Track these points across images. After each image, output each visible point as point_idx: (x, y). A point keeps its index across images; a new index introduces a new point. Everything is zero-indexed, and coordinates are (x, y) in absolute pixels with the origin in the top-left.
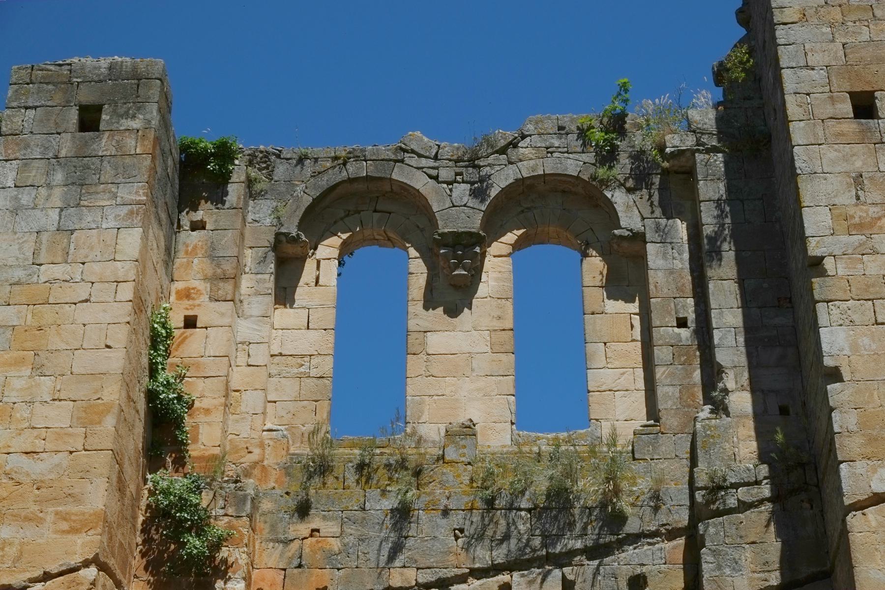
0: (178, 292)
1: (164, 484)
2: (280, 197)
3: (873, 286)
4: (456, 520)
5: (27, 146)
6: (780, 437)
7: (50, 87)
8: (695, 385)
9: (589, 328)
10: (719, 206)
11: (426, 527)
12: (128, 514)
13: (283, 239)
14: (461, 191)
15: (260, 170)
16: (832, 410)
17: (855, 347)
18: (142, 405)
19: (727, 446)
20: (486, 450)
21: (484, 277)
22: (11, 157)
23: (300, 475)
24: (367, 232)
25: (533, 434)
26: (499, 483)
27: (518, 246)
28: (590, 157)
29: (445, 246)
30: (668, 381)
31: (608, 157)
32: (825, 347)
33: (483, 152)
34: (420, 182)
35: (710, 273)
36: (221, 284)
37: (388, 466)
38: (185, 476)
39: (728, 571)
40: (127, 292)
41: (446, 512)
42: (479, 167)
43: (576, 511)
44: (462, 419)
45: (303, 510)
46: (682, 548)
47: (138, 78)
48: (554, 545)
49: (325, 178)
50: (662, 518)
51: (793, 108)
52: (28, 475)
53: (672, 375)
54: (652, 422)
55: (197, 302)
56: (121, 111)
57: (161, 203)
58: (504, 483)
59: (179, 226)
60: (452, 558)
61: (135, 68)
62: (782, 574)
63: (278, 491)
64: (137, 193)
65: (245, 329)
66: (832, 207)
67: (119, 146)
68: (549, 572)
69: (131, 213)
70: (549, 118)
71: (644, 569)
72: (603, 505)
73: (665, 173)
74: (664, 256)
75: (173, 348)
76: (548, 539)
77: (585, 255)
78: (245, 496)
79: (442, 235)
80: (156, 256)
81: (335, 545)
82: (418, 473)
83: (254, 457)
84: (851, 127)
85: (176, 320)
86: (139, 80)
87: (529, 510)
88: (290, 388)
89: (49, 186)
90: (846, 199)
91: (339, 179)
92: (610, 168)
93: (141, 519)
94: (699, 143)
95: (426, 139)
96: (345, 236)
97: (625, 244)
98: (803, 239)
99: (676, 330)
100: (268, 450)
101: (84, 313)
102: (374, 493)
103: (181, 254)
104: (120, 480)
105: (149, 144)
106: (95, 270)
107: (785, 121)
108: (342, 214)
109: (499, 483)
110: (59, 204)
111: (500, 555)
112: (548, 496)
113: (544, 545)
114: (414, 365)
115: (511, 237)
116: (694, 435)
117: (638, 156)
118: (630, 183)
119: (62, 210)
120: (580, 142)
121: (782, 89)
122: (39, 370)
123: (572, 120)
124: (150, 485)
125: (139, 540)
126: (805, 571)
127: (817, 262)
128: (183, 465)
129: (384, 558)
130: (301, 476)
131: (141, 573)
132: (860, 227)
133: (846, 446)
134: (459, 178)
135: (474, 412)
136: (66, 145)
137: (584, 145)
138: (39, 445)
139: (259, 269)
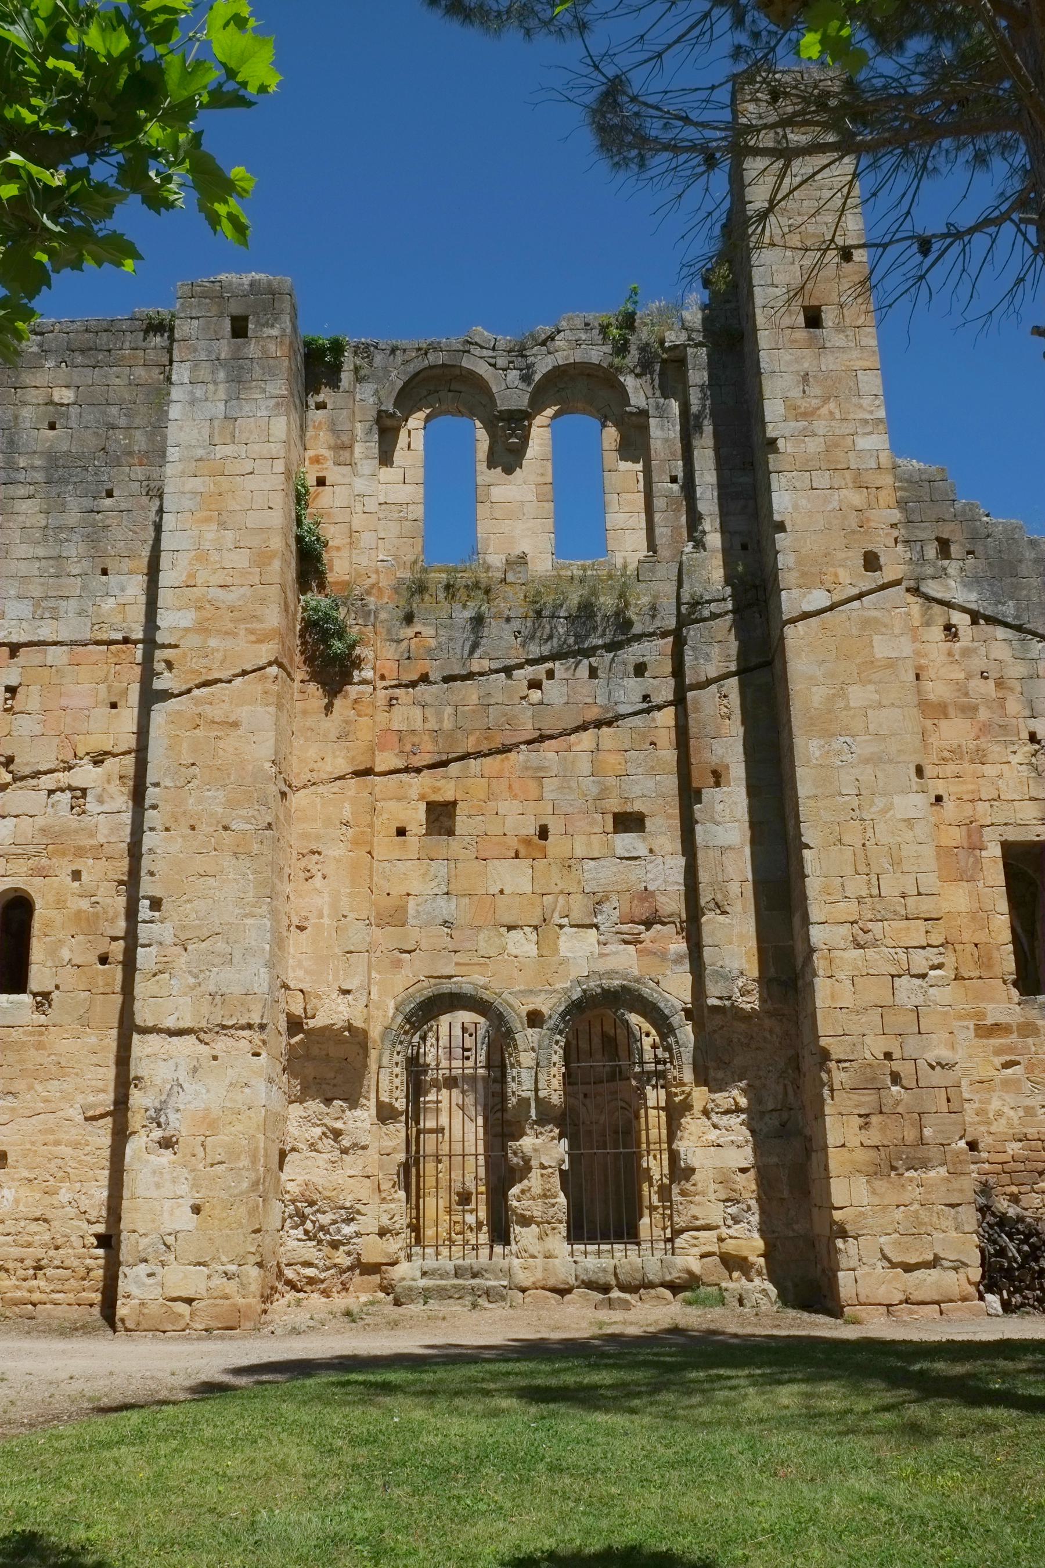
0: (310, 458)
1: (313, 603)
2: (379, 380)
3: (812, 460)
4: (516, 625)
5: (195, 350)
6: (740, 569)
7: (208, 301)
8: (681, 527)
9: (607, 482)
10: (702, 391)
11: (495, 631)
12: (291, 625)
13: (384, 415)
14: (513, 375)
15: (363, 358)
16: (778, 552)
17: (796, 507)
18: (294, 548)
19: (704, 572)
20: (534, 574)
21: (530, 442)
22: (185, 359)
23: (405, 593)
24: (444, 407)
25: (567, 562)
26: (545, 599)
27: (554, 417)
28: (608, 349)
29: (503, 420)
30: (663, 524)
31: (621, 349)
32: (775, 507)
33: (530, 343)
34: (483, 369)
35: (695, 443)
36: (341, 452)
37: (467, 587)
38: (326, 596)
39: (702, 661)
40: (279, 466)
41: (508, 620)
42: (526, 356)
43: (598, 619)
44: (518, 552)
45: (409, 619)
46: (671, 644)
47: (273, 293)
48: (583, 642)
49: (412, 366)
50: (658, 623)
51: (760, 320)
52: (224, 602)
53: (666, 519)
54: (651, 553)
55: (325, 466)
56: (263, 321)
57: (296, 392)
58: (549, 599)
59: (307, 406)
60: (513, 651)
61: (269, 283)
62: (738, 664)
63: (391, 605)
64: (280, 388)
65: (360, 485)
66: (786, 399)
67: (264, 350)
68: (580, 661)
69: (278, 404)
70: (578, 316)
71: (645, 659)
72: (617, 614)
73: (664, 362)
74: (662, 429)
75: (310, 502)
76: (579, 638)
77: (604, 426)
78: (370, 611)
79: (500, 412)
80: (295, 433)
81: (433, 643)
82: (487, 592)
83: (373, 579)
84: (802, 334)
85: (311, 481)
86: (274, 295)
87: (566, 618)
88: (394, 528)
89: (215, 383)
90: (796, 393)
91: (422, 366)
92: (624, 358)
93: (298, 627)
94: (690, 339)
95: (486, 333)
96: (428, 411)
97: (634, 418)
98: (763, 424)
99: (670, 485)
100: (382, 576)
101: (250, 483)
102: (458, 606)
103: (310, 429)
104: (286, 604)
105: (286, 348)
106: (256, 449)
107: (755, 330)
108: (425, 393)
109: (545, 599)
110: (224, 397)
111: (546, 650)
112: (579, 608)
113: (576, 643)
114: (482, 510)
115: (550, 412)
116: (681, 564)
117: (644, 349)
118: (638, 370)
119: (226, 402)
120: (601, 336)
121: (753, 303)
122: (223, 526)
123: (595, 317)
124: (302, 603)
125: (299, 642)
126: (754, 661)
127: (773, 442)
128: (324, 588)
129: (466, 653)
130: (406, 594)
131: (301, 665)
132: (807, 415)
133: (787, 578)
134: (511, 366)
135: (524, 546)
136: (224, 348)
137: (604, 338)
138: (229, 581)
139: (367, 439)
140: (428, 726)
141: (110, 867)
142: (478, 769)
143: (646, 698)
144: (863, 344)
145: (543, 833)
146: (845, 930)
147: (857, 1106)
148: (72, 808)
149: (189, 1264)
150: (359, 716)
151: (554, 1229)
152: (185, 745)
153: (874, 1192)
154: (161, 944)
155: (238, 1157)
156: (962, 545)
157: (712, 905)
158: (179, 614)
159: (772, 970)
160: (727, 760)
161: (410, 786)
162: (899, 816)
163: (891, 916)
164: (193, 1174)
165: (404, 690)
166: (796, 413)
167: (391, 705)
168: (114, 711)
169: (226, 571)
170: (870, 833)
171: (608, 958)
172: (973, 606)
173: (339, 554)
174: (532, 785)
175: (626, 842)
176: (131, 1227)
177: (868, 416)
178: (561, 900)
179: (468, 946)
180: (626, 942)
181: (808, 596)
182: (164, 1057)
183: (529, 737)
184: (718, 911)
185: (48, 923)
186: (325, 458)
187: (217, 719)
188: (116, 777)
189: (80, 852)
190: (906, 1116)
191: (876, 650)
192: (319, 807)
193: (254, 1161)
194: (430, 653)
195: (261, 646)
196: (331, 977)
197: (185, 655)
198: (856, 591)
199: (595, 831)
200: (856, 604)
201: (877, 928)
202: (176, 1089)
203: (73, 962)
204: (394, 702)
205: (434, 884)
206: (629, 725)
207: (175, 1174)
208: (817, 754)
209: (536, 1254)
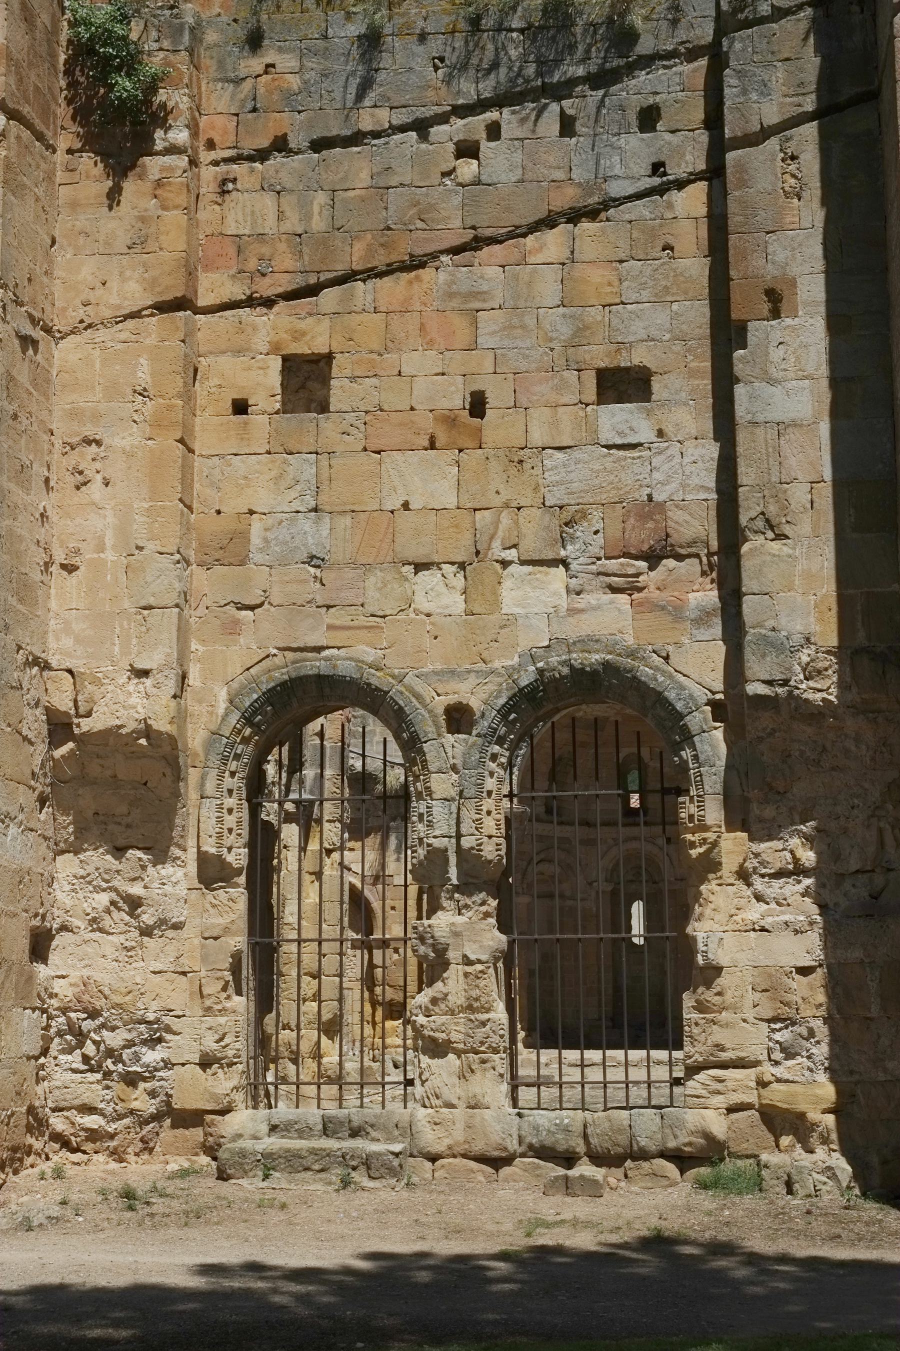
81: (294, 82)
140: (287, 226)
142: (370, 298)
143: (657, 168)
150: (164, 208)
151: (484, 1062)
157: (760, 524)
160: (794, 270)
165: (246, 165)
167: (224, 193)
171: (583, 616)
178: (506, 519)
179: (349, 596)
180: (614, 590)
183: (457, 241)
184: (770, 535)
199: (565, 400)
205: (293, 494)
206: (627, 217)
209: (455, 1101)
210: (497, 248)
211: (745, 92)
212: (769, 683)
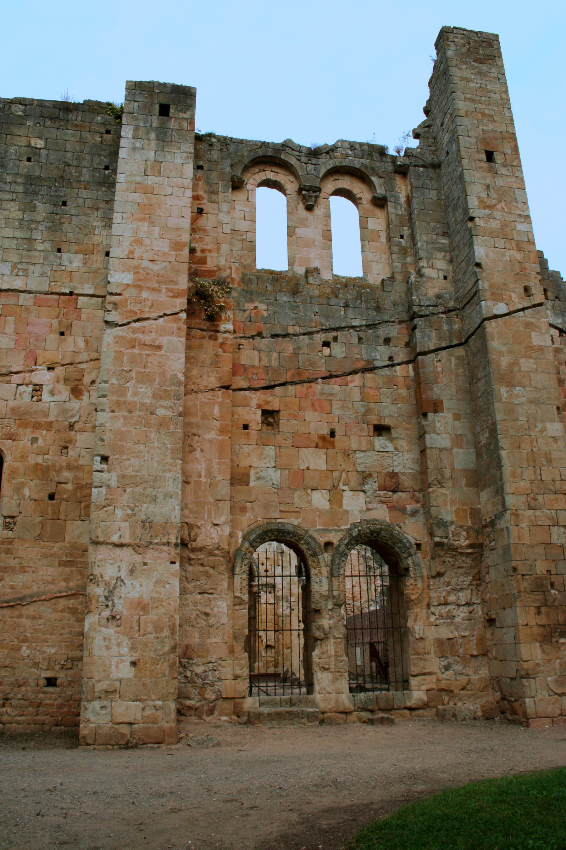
17: (487, 256)
32: (476, 254)
39: (426, 339)
52: (152, 270)
66: (479, 198)
69: (188, 157)
81: (265, 314)
84: (485, 165)
89: (149, 140)
90: (484, 195)
108: (257, 171)
132: (489, 207)
136: (155, 121)
138: (156, 258)
140: (263, 363)
141: (58, 437)
142: (293, 392)
143: (391, 358)
144: (517, 175)
145: (333, 434)
146: (523, 498)
147: (533, 602)
148: (33, 397)
149: (130, 701)
150: (224, 352)
151: (342, 675)
152: (125, 357)
153: (544, 652)
154: (109, 486)
155: (162, 630)
156: (553, 293)
157: (436, 482)
158: (123, 275)
159: (469, 522)
160: (442, 398)
161: (251, 398)
162: (549, 435)
163: (548, 491)
164: (132, 640)
165: (247, 340)
166: (483, 204)
167: (239, 349)
168: (63, 337)
169: (154, 252)
170: (535, 444)
171: (372, 512)
172: (560, 326)
173: (211, 255)
174: (326, 404)
175: (380, 442)
176: (89, 675)
177: (522, 213)
178: (344, 475)
179: (288, 500)
180: (383, 502)
181: (497, 306)
182: (111, 562)
183: (324, 375)
184: (439, 486)
185: (14, 472)
186: (203, 198)
187: (147, 343)
188: (62, 379)
189: (37, 426)
190: (559, 607)
191: (533, 340)
192: (199, 407)
193: (173, 633)
194: (265, 320)
195: (176, 299)
196: (206, 516)
197: (126, 300)
198: (520, 306)
199: (363, 434)
200: (521, 313)
201: (540, 498)
202: (119, 583)
203: (32, 498)
204: (241, 347)
205: (266, 461)
206: (382, 373)
207: (119, 640)
208: (506, 395)
209: (331, 691)
210: (338, 379)
211: (423, 338)
212: (442, 537)
